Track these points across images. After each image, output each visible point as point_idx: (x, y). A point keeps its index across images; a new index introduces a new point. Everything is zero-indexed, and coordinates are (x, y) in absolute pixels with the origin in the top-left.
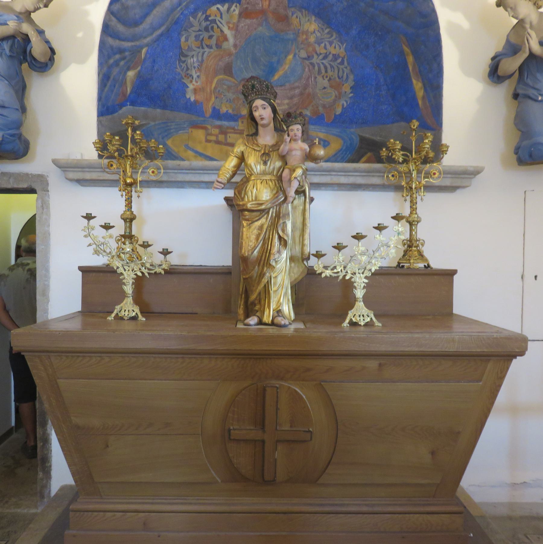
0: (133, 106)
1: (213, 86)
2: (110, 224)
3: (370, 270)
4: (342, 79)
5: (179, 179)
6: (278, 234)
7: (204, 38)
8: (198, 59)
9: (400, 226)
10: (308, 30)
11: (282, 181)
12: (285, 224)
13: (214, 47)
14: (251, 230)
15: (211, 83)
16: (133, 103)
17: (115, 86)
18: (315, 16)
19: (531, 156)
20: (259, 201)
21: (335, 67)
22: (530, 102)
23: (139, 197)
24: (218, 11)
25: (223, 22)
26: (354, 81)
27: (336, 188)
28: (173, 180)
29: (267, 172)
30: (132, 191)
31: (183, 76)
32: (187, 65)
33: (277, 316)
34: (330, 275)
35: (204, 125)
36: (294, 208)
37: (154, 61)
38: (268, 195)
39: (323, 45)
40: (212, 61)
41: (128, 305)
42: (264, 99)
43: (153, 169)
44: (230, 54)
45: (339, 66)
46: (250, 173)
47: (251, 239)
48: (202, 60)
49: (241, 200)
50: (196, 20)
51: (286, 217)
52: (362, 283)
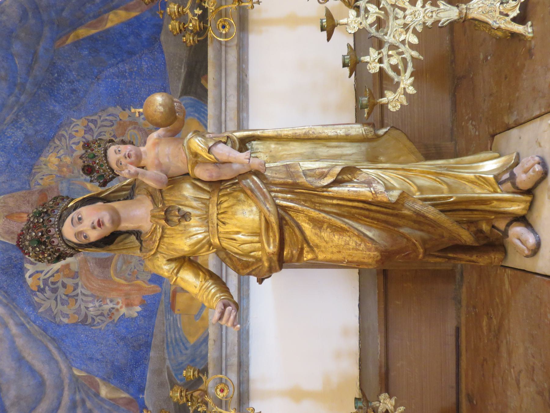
0: (144, 389)
1: (123, 282)
5: (236, 339)
8: (91, 302)
10: (56, 165)
11: (221, 181)
12: (308, 172)
13: (76, 281)
14: (323, 244)
15: (119, 284)
16: (141, 390)
20: (260, 229)
21: (99, 131)
24: (33, 277)
26: (115, 106)
28: (236, 348)
31: (111, 320)
32: (97, 316)
33: (514, 184)
34: (411, 76)
36: (274, 159)
37: (91, 359)
38: (249, 209)
39: (74, 146)
40: (93, 283)
42: (61, 220)
43: (218, 390)
44: (86, 261)
45: (98, 125)
46: (207, 246)
47: (343, 243)
48: (92, 296)
49: (260, 264)
50: (43, 304)
51: (292, 170)
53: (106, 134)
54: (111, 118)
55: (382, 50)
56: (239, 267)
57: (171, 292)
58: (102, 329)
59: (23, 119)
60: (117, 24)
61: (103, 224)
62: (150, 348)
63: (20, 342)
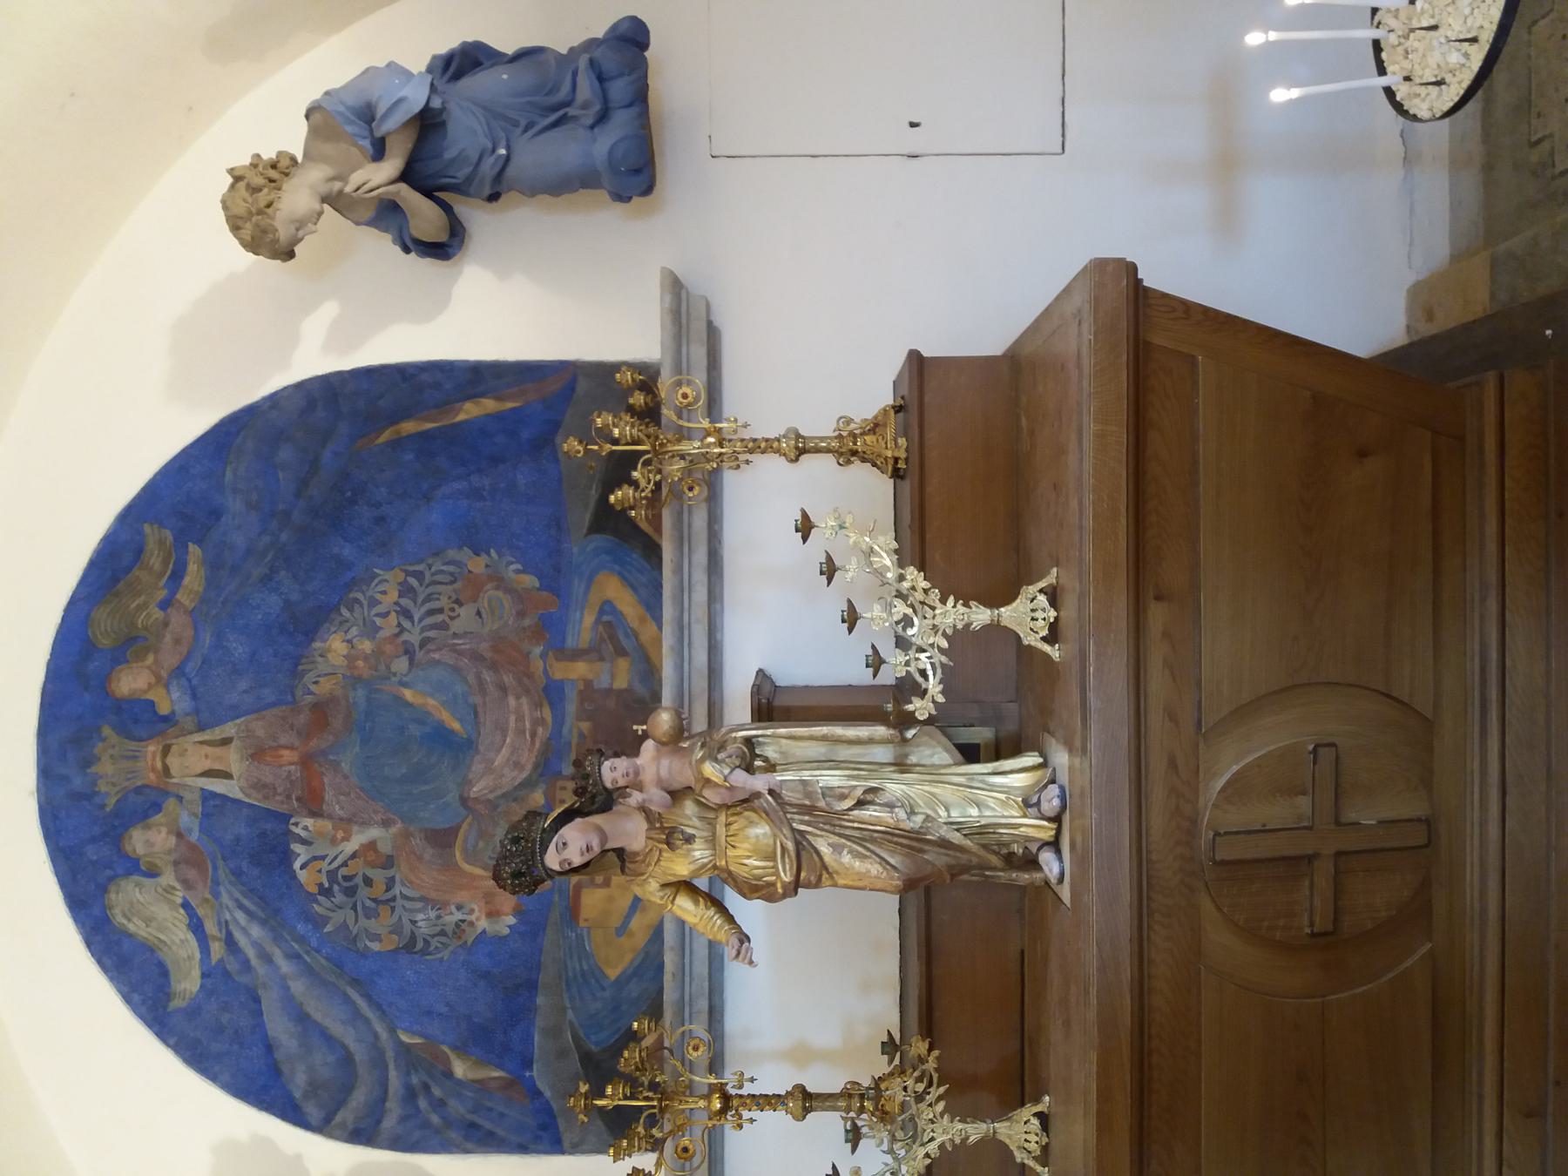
2: (821, 564)
3: (926, 591)
4: (456, 575)
6: (850, 809)
8: (419, 911)
10: (344, 657)
13: (390, 873)
15: (473, 877)
16: (527, 1064)
17: (490, 1110)
18: (313, 640)
19: (637, 171)
22: (511, 171)
23: (752, 1080)
24: (308, 867)
25: (332, 853)
26: (460, 548)
27: (718, 606)
28: (706, 984)
29: (710, 834)
30: (741, 1096)
32: (433, 936)
33: (1039, 811)
34: (940, 683)
37: (429, 1013)
39: (378, 621)
41: (1013, 1132)
42: (544, 849)
43: (690, 1048)
44: (406, 835)
45: (427, 581)
48: (423, 899)
51: (810, 789)
52: (955, 610)
53: (441, 597)
54: (451, 568)
55: (910, 652)
56: (746, 891)
57: (571, 886)
59: (283, 573)
61: (592, 849)
62: (536, 988)
63: (298, 987)
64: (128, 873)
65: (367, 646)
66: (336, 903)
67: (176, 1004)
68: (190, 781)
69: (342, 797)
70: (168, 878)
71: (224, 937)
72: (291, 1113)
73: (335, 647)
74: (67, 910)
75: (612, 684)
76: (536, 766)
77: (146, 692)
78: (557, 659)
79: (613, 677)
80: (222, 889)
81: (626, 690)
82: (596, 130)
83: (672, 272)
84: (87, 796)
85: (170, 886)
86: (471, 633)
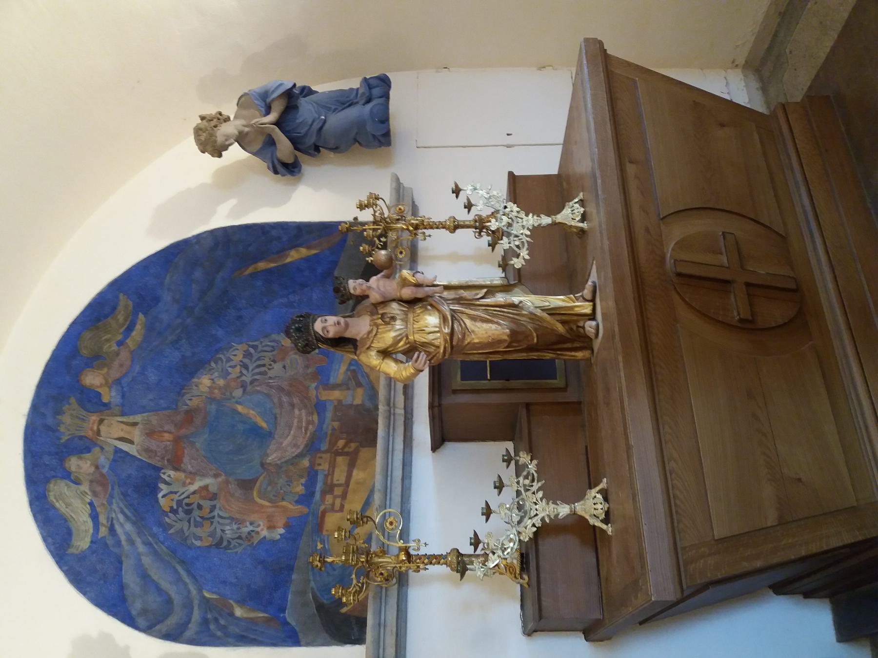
1: (267, 504)
2: (471, 538)
3: (518, 212)
6: (482, 298)
7: (200, 515)
8: (227, 525)
9: (466, 189)
10: (208, 387)
15: (262, 506)
16: (283, 610)
17: (256, 630)
18: (193, 377)
22: (326, 126)
24: (166, 497)
25: (182, 490)
26: (279, 333)
32: (233, 539)
35: (319, 515)
37: (224, 582)
39: (230, 370)
44: (227, 482)
50: (174, 526)
55: (510, 238)
57: (320, 512)
58: (239, 552)
60: (296, 260)
62: (292, 570)
63: (147, 560)
64: (63, 478)
65: (221, 382)
66: (179, 518)
67: (70, 551)
68: (109, 440)
69: (193, 461)
70: (85, 487)
71: (109, 526)
72: (129, 620)
73: (204, 382)
74: (25, 483)
75: (353, 402)
76: (306, 446)
77: (98, 387)
78: (324, 389)
79: (354, 398)
80: (114, 501)
81: (361, 405)
82: (366, 105)
83: (396, 175)
84: (52, 430)
85: (85, 492)
86: (279, 377)
